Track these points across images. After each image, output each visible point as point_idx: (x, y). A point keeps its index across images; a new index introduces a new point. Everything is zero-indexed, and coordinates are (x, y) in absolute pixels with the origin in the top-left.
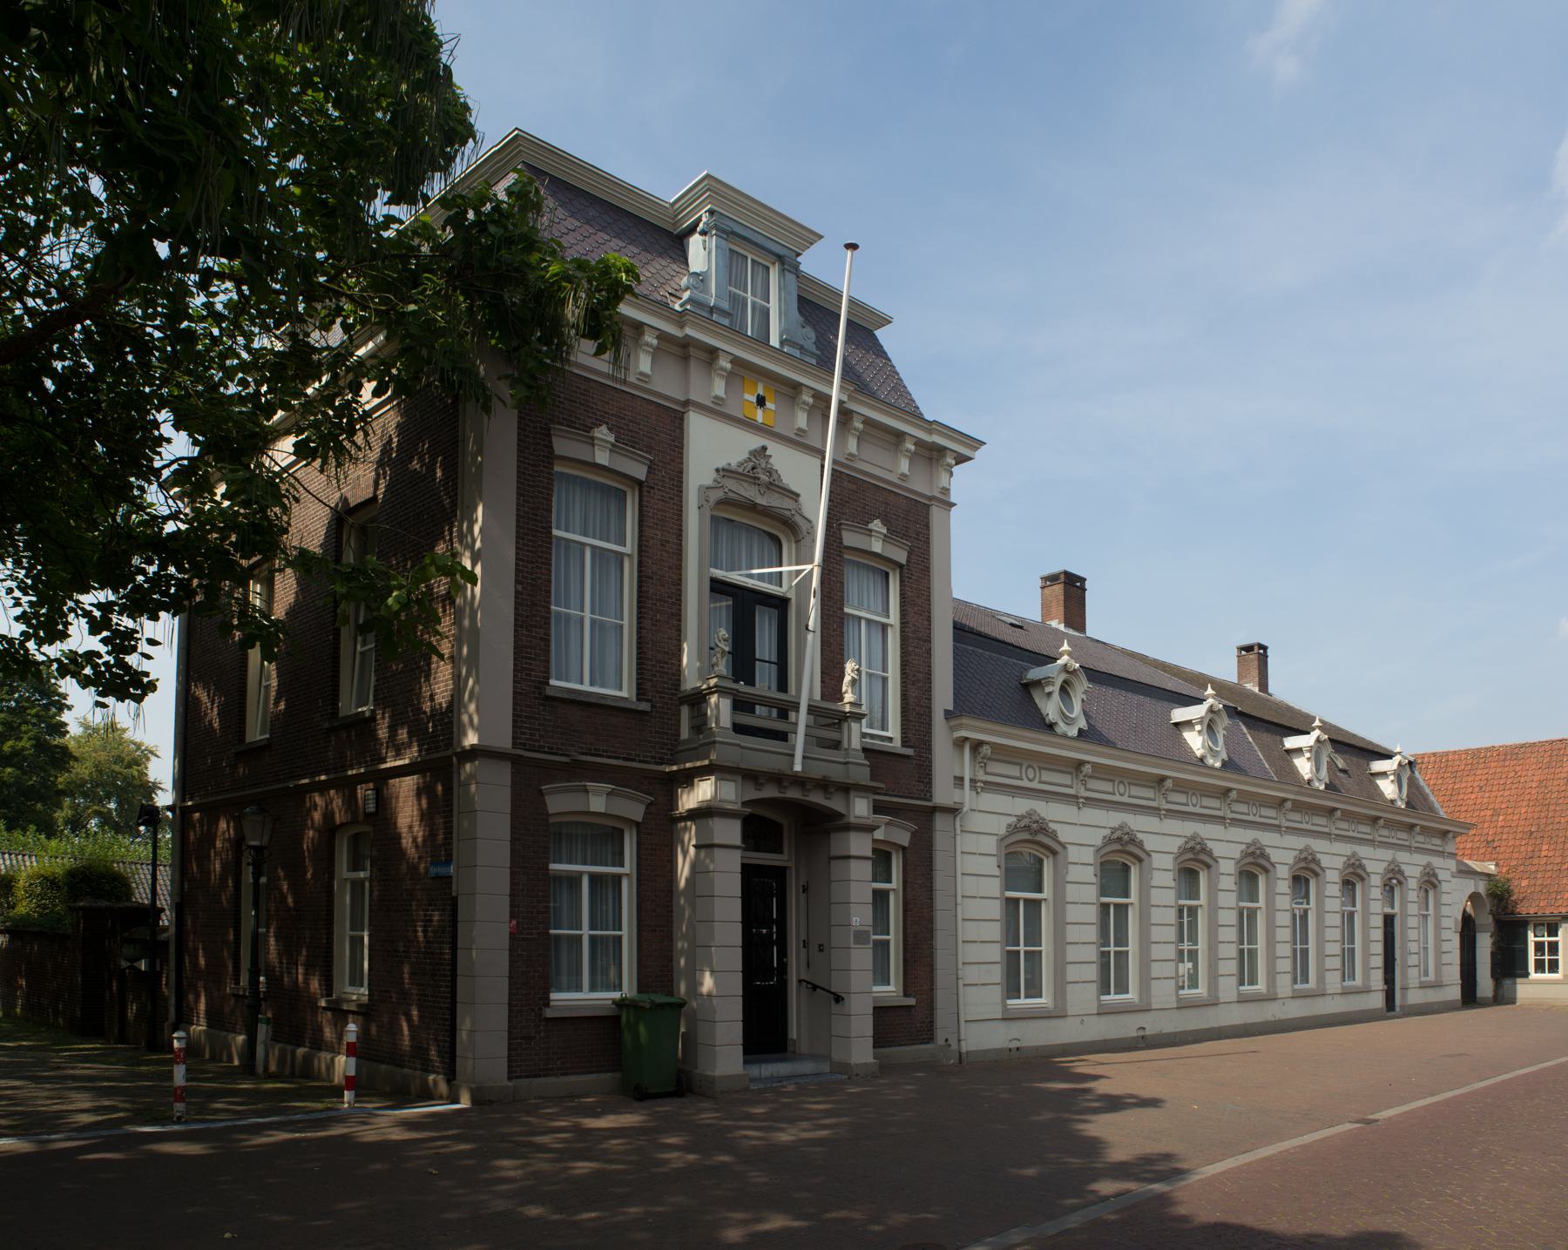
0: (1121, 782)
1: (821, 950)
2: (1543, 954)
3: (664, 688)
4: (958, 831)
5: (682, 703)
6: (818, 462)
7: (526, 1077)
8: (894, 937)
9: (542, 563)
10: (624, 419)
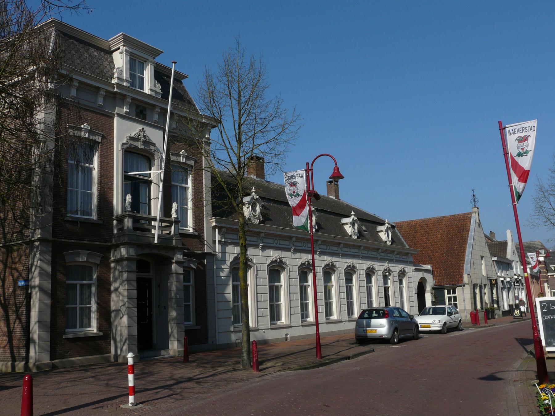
0: (328, 245)
1: (165, 308)
2: (273, 302)
4: (214, 260)
6: (162, 133)
8: (192, 303)
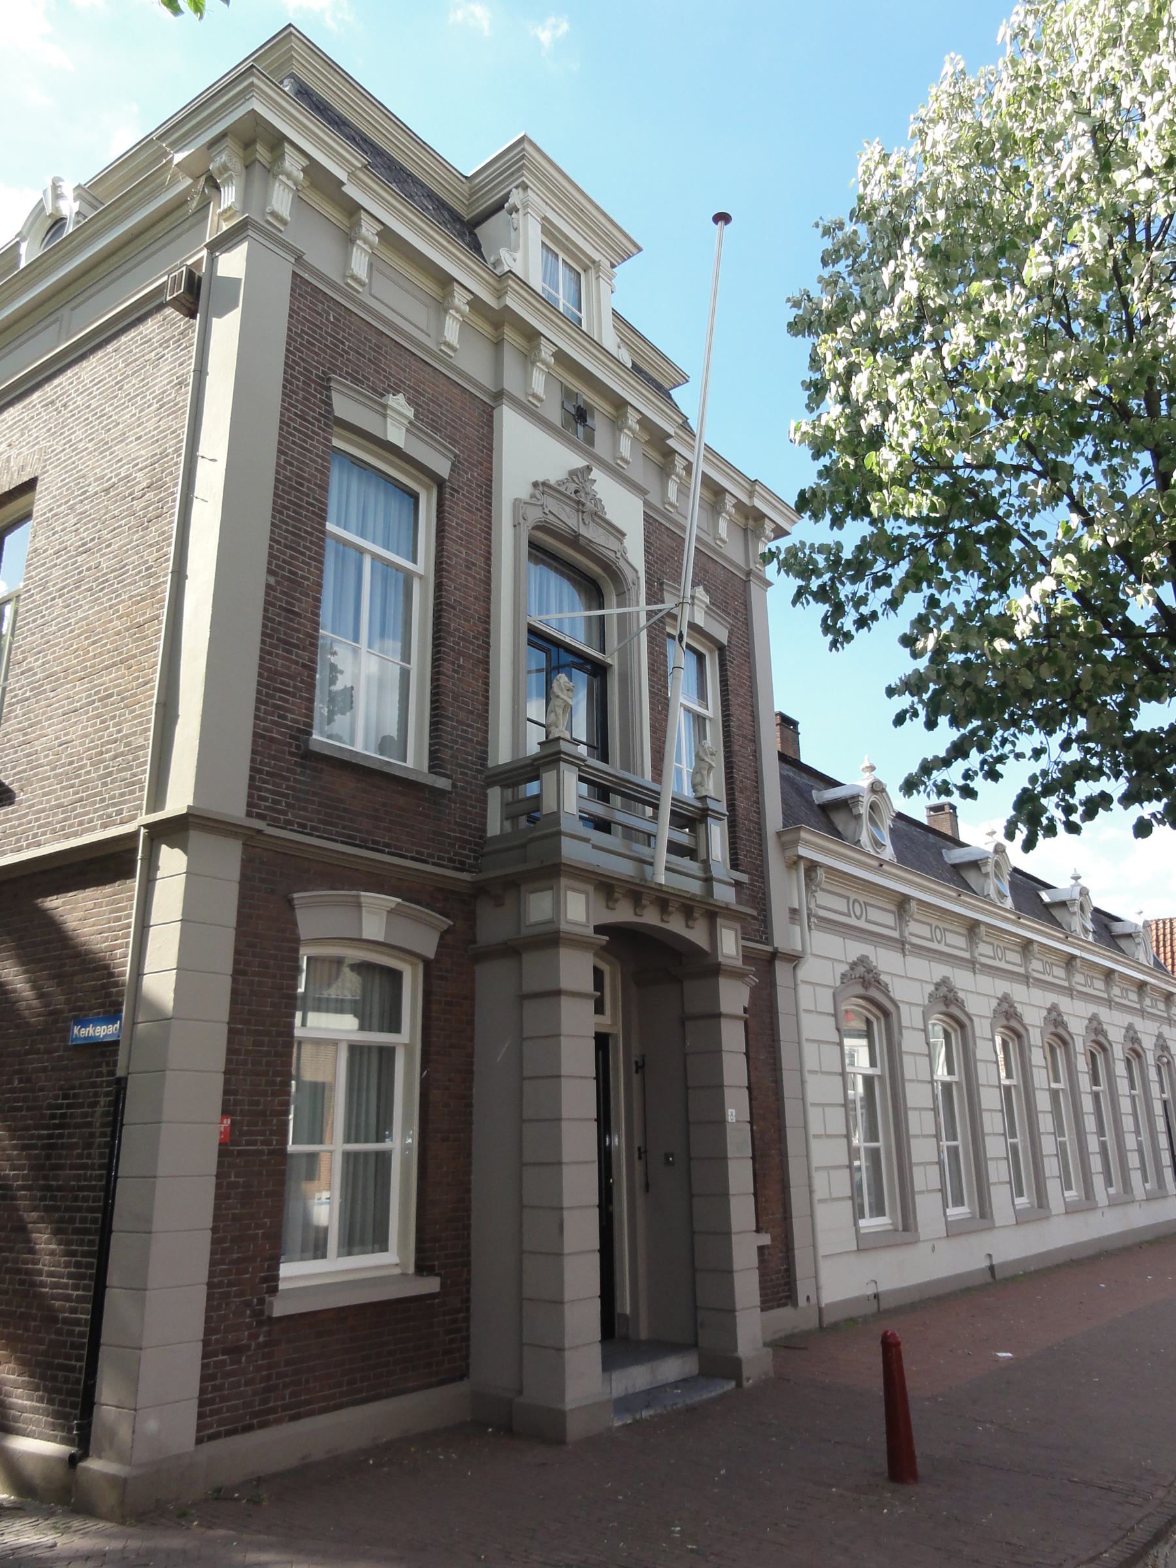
1: (668, 1163)
3: (466, 760)
5: (490, 784)
7: (229, 1433)
9: (311, 558)
10: (423, 395)
